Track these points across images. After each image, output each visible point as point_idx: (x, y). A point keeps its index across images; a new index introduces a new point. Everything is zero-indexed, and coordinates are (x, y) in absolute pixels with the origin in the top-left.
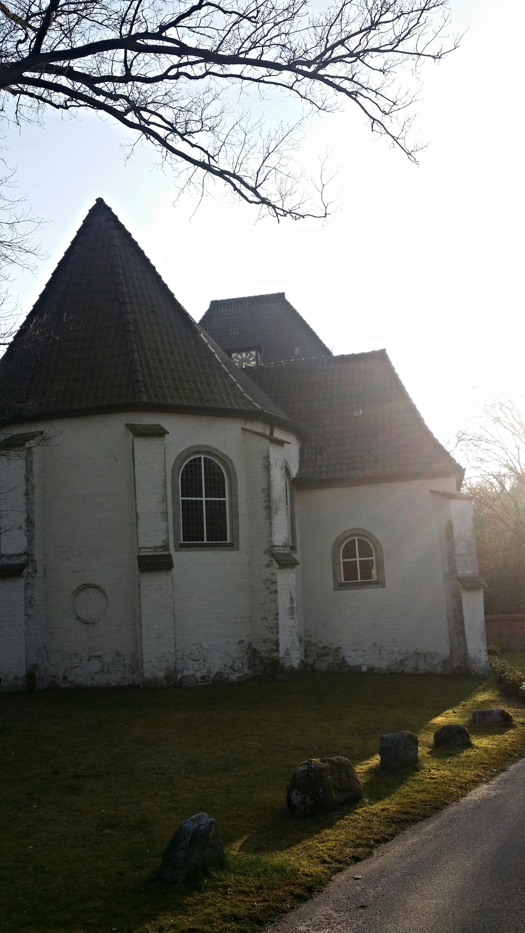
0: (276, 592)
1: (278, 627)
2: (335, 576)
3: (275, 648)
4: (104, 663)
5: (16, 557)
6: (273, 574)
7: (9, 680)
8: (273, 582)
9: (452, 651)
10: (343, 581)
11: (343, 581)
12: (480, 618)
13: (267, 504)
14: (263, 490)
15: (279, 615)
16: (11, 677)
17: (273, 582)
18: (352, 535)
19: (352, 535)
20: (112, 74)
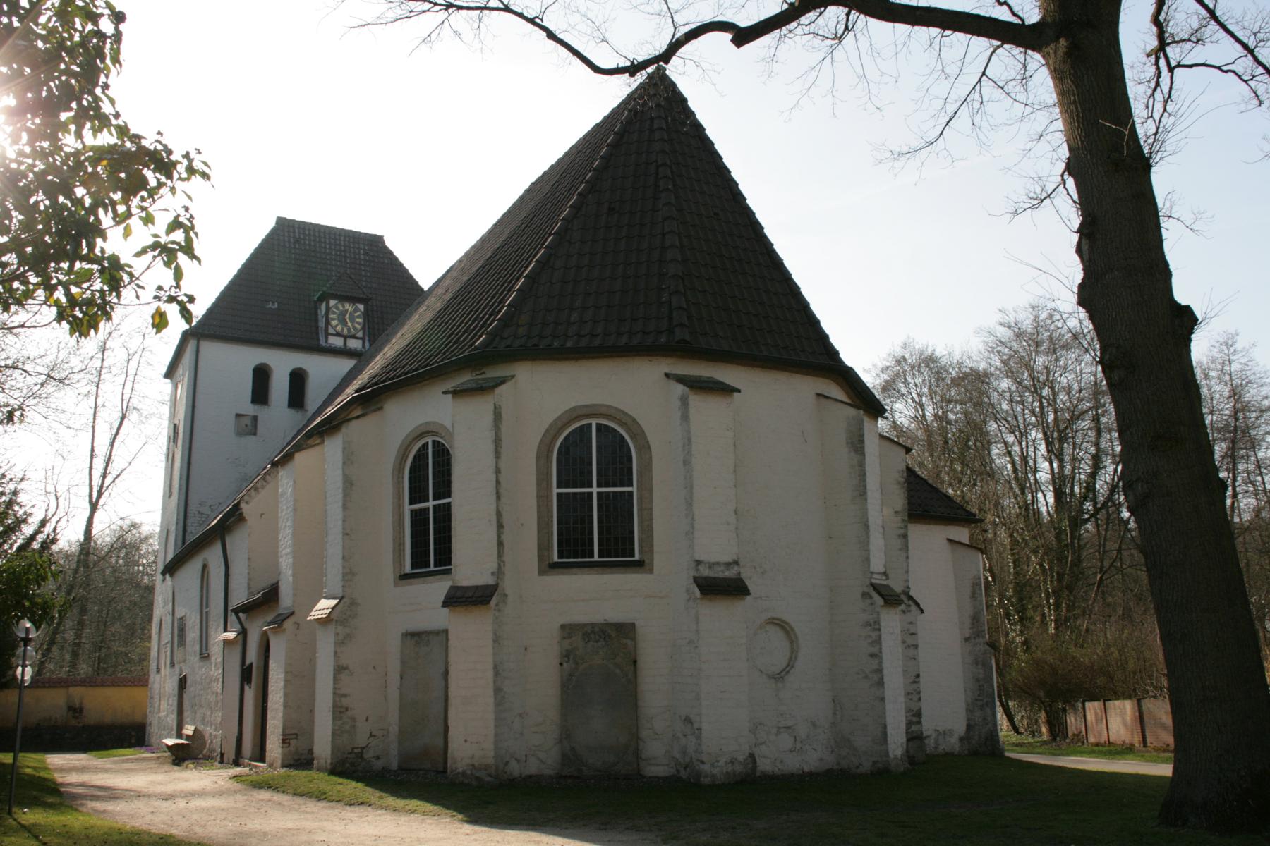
0: (916, 647)
1: (919, 693)
2: (543, 547)
3: (915, 719)
4: (795, 737)
5: (722, 568)
6: (911, 623)
7: (720, 764)
8: (912, 634)
9: (969, 727)
10: (556, 559)
11: (556, 559)
12: (244, 582)
13: (902, 531)
14: (896, 512)
15: (922, 679)
16: (723, 760)
17: (912, 634)
18: (422, 435)
19: (422, 435)
20: (848, 14)
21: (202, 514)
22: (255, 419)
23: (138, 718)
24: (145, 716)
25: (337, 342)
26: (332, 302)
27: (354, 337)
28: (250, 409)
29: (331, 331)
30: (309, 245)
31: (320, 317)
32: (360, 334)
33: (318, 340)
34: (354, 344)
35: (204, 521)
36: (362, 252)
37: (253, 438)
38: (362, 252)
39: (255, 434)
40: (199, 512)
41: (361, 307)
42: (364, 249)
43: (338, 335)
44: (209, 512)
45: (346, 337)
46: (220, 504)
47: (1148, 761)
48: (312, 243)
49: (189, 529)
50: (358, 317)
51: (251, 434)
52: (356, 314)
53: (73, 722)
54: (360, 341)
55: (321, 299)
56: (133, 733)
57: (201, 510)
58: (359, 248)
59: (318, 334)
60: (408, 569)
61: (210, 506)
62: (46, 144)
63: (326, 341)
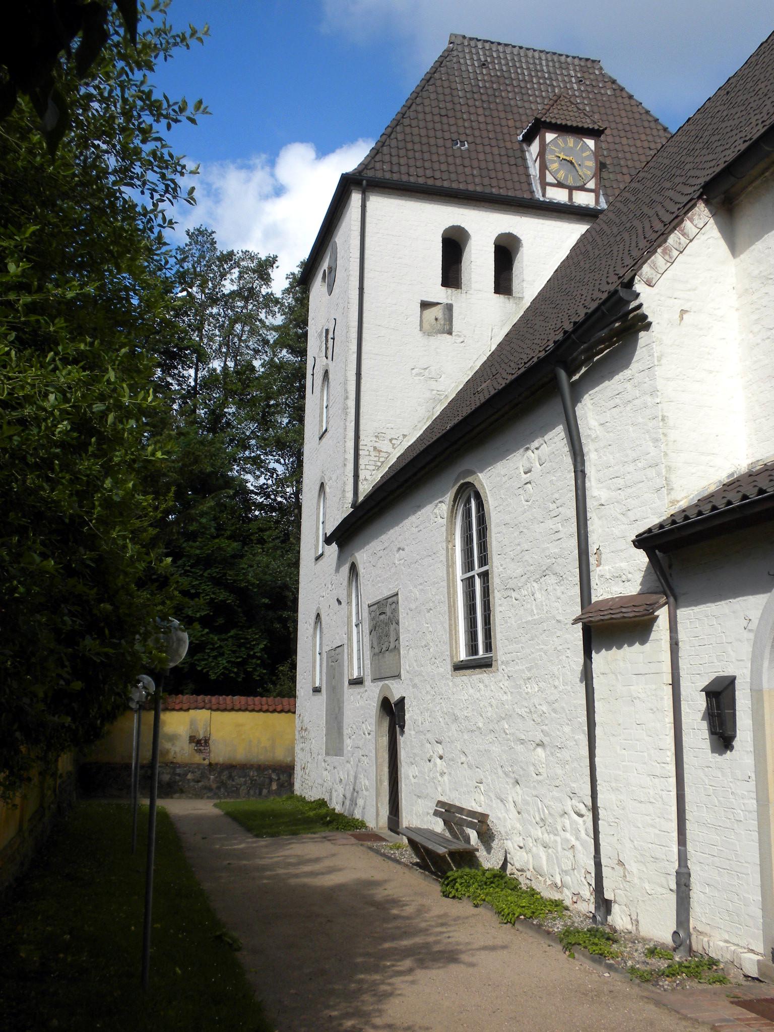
21: (380, 451)
22: (449, 308)
23: (280, 755)
24: (291, 751)
25: (559, 195)
26: (550, 137)
27: (582, 188)
28: (441, 294)
29: (550, 179)
30: (502, 70)
31: (530, 163)
32: (591, 185)
33: (532, 192)
34: (584, 199)
35: (382, 462)
36: (573, 80)
37: (448, 336)
38: (573, 80)
39: (450, 333)
40: (375, 448)
41: (591, 143)
42: (576, 76)
43: (560, 185)
44: (390, 450)
45: (571, 189)
46: (405, 436)
47: (191, 798)
48: (504, 68)
49: (362, 474)
50: (587, 158)
51: (443, 332)
52: (584, 155)
53: (198, 759)
54: (593, 195)
55: (528, 139)
56: (274, 776)
57: (376, 445)
58: (569, 75)
59: (530, 184)
60: (463, 655)
61: (391, 440)
62: (149, 479)
63: (544, 195)
